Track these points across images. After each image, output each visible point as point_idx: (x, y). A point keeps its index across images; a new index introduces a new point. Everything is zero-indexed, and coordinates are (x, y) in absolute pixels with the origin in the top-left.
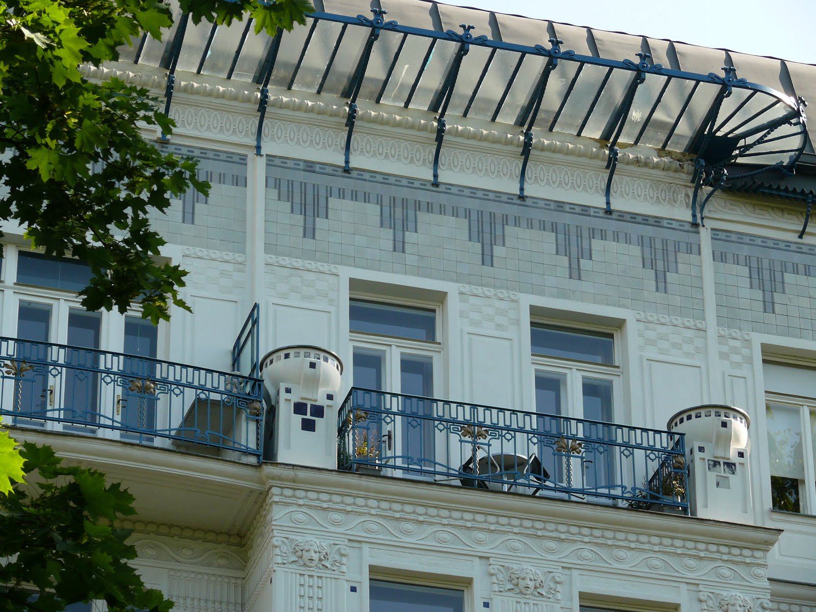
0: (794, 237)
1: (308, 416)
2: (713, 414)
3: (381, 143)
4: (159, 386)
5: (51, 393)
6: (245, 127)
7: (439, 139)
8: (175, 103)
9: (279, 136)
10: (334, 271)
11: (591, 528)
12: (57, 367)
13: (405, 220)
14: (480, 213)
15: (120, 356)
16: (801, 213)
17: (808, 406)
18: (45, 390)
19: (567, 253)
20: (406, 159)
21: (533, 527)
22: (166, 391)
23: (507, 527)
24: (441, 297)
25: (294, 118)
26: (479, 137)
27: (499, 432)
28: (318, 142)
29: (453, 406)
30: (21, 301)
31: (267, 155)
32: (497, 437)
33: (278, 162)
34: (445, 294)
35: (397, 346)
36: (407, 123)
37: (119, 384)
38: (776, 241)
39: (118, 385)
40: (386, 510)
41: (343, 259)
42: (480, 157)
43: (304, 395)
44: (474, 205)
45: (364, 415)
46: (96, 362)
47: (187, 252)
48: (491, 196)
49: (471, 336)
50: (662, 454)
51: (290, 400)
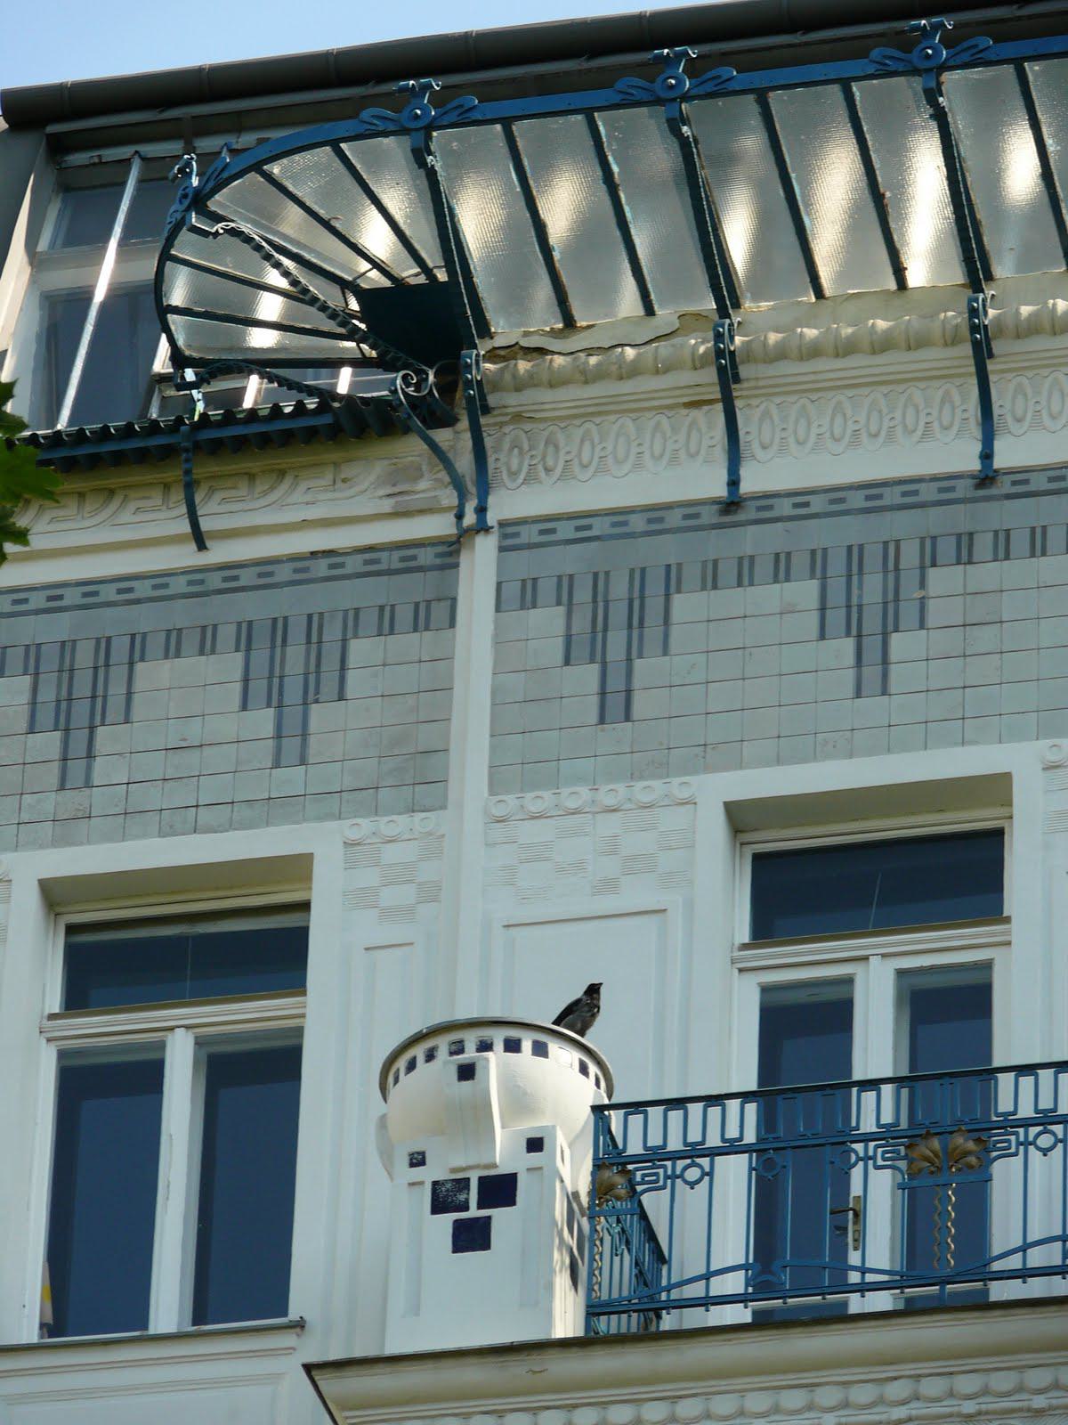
0: (187, 556)
1: (474, 1212)
2: (527, 1045)
3: (838, 408)
4: (639, 1174)
5: (856, 1215)
6: (1031, 403)
7: (982, 351)
8: (1003, 371)
9: (585, 460)
10: (684, 794)
11: (844, 1383)
12: (698, 1160)
13: (891, 602)
14: (599, 581)
15: (690, 1106)
16: (167, 487)
17: (187, 1027)
18: (840, 1211)
19: (596, 653)
20: (909, 432)
21: (1020, 1389)
22: (1013, 1150)
23: (1016, 1397)
24: (997, 788)
25: (819, 377)
26: (1047, 326)
27: (664, 1167)
28: (801, 438)
29: (695, 1109)
30: (901, 973)
31: (502, 524)
32: (661, 1183)
33: (529, 534)
34: (1006, 778)
35: (884, 956)
36: (800, 348)
37: (880, 1162)
38: (124, 582)
39: (877, 1168)
40: (1008, 1394)
41: (709, 756)
42: (804, 407)
43: (460, 1161)
44: (570, 560)
45: (971, 1145)
46: (767, 1122)
47: (1053, 757)
48: (818, 504)
49: (513, 931)
50: (877, 1147)
51: (422, 1183)
